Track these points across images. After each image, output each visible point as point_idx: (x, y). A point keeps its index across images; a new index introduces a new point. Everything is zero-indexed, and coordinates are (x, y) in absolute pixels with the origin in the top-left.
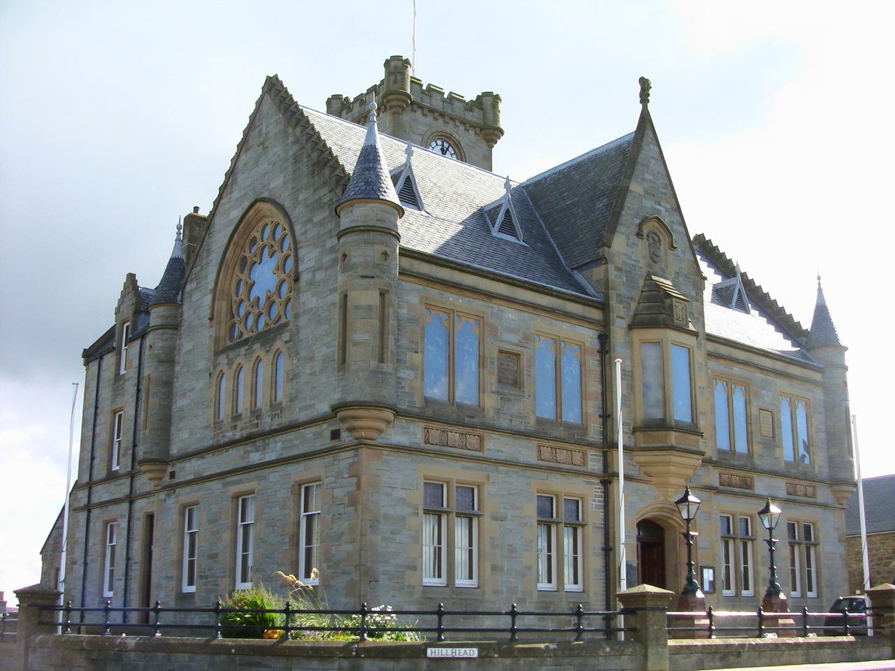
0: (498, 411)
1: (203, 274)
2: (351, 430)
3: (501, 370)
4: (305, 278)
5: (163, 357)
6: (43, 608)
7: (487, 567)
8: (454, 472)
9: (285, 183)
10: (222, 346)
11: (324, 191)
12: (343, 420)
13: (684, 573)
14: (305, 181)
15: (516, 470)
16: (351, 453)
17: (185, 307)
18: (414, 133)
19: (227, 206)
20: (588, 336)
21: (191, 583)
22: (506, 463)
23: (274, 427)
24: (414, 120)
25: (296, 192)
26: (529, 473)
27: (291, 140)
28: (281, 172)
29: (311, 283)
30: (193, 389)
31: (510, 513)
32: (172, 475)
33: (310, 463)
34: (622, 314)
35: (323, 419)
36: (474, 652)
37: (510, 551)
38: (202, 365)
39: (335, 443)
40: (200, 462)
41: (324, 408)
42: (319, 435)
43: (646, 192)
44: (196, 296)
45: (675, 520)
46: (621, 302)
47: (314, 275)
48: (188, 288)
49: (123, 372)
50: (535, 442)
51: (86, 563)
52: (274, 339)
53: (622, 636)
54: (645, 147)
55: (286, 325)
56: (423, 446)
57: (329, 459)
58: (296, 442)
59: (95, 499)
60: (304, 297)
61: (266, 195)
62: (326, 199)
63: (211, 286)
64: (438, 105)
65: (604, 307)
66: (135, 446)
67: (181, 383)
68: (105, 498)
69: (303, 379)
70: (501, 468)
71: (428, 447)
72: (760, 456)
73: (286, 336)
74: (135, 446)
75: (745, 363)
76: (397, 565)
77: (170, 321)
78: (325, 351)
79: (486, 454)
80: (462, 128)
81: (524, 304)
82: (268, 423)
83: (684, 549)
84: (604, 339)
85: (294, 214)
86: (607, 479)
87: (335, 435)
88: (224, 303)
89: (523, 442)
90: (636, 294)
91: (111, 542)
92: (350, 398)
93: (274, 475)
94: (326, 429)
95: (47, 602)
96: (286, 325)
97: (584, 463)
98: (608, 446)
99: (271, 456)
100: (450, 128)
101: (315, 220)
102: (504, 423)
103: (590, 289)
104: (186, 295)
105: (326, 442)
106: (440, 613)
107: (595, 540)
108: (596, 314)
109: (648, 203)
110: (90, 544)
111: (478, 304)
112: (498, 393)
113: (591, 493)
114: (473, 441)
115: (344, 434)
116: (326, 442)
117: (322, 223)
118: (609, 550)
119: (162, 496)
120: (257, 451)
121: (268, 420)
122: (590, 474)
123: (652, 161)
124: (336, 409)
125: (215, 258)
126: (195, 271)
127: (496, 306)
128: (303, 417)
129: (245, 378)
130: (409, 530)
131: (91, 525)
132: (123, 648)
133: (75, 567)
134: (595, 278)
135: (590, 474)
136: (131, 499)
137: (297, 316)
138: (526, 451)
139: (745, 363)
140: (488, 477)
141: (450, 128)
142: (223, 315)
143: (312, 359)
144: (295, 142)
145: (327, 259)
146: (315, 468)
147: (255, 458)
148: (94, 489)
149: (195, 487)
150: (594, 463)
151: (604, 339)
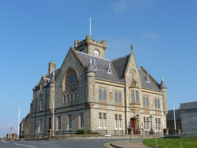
3: (110, 96)
7: (108, 125)
8: (103, 111)
13: (137, 126)
20: (123, 89)
26: (113, 111)
36: (110, 136)
45: (136, 111)
49: (42, 93)
51: (35, 127)
53: (128, 134)
54: (132, 57)
55: (77, 89)
56: (99, 108)
65: (125, 85)
66: (46, 106)
68: (39, 115)
72: (151, 107)
73: (77, 90)
74: (46, 106)
75: (148, 92)
79: (107, 109)
80: (92, 45)
82: (74, 104)
83: (137, 123)
84: (125, 90)
86: (126, 112)
90: (130, 82)
96: (77, 89)
97: (122, 110)
98: (126, 107)
99: (74, 109)
100: (97, 48)
102: (110, 104)
105: (84, 107)
106: (115, 131)
107: (124, 121)
108: (124, 86)
109: (132, 67)
110: (36, 123)
111: (106, 86)
113: (123, 114)
116: (84, 107)
118: (126, 123)
122: (123, 111)
127: (109, 86)
128: (80, 103)
129: (74, 99)
135: (123, 111)
136: (45, 115)
137: (79, 88)
138: (113, 108)
139: (148, 92)
143: (82, 95)
147: (71, 109)
150: (124, 109)
151: (125, 90)
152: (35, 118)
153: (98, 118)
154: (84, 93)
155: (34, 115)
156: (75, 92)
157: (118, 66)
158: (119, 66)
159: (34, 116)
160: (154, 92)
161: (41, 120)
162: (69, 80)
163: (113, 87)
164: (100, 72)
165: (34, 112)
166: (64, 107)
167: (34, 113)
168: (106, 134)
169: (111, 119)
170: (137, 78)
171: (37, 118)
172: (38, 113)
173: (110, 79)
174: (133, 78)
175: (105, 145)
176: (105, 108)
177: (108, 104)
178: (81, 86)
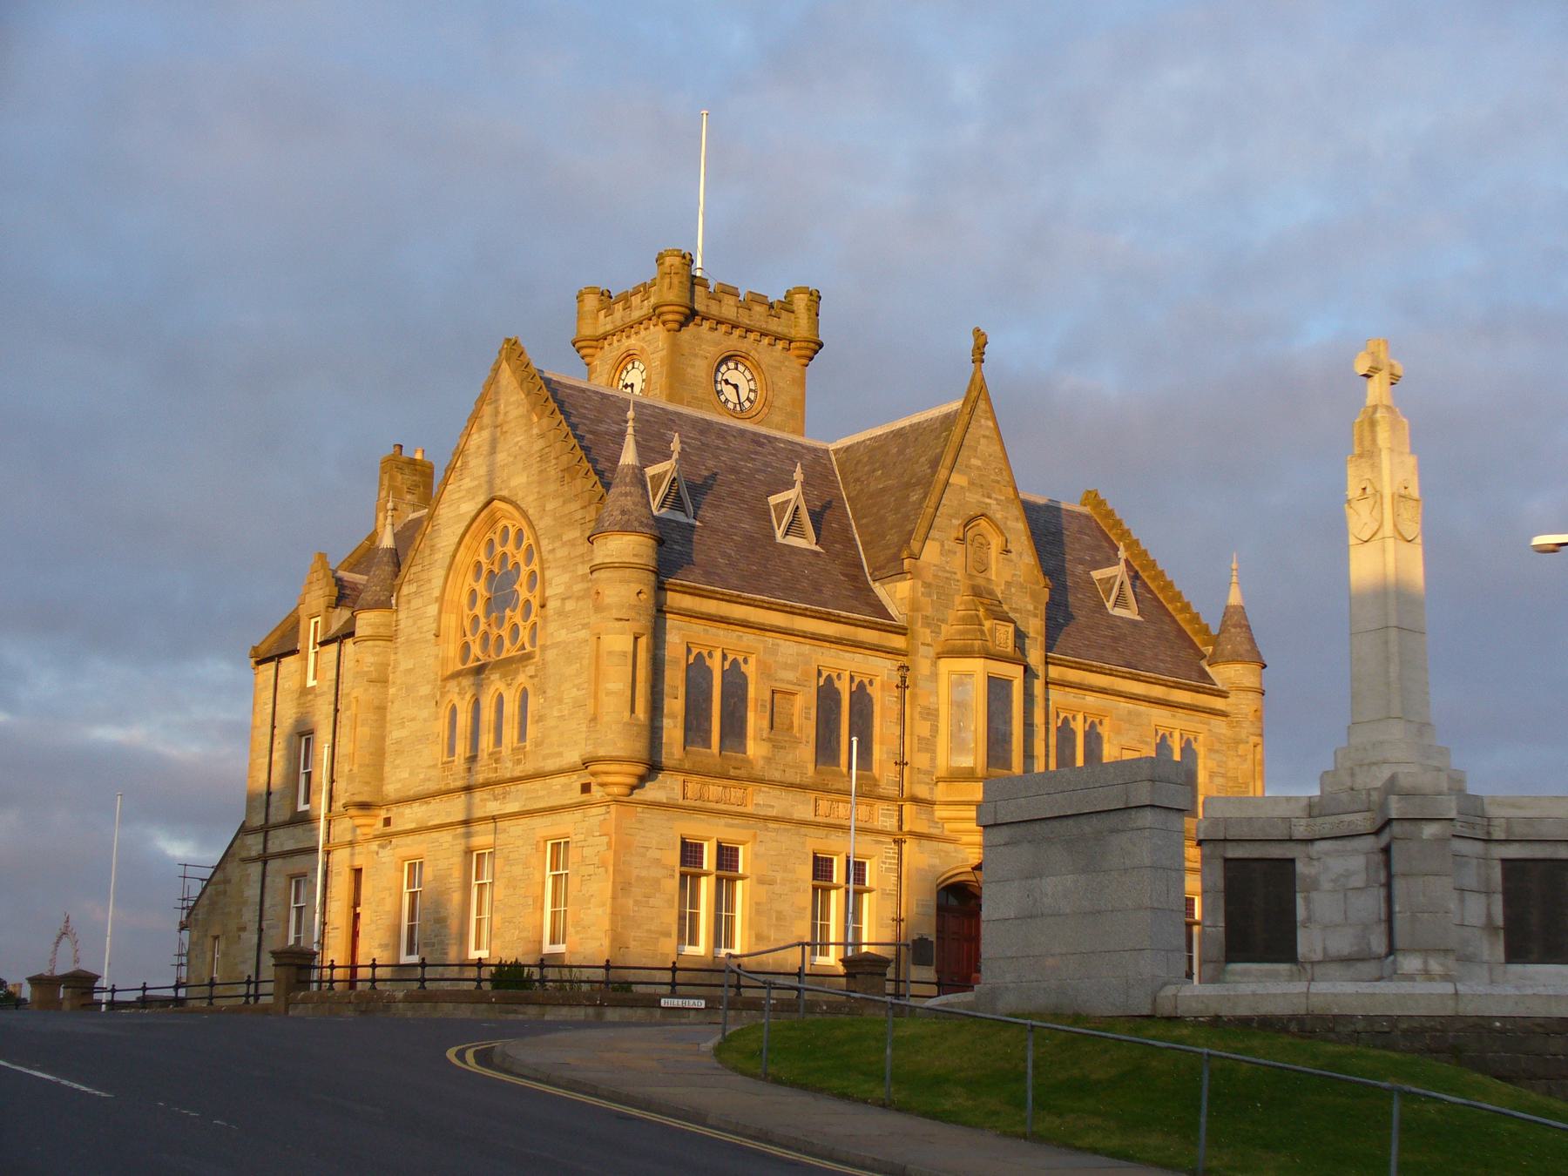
0: (768, 760)
1: (425, 576)
2: (602, 785)
4: (552, 605)
5: (374, 675)
6: (300, 967)
9: (528, 483)
10: (451, 669)
11: (574, 506)
12: (593, 774)
14: (552, 487)
15: (788, 826)
16: (603, 810)
17: (402, 615)
18: (696, 355)
19: (456, 496)
21: (410, 952)
22: (776, 819)
23: (517, 774)
24: (698, 338)
25: (542, 498)
26: (804, 830)
27: (535, 431)
28: (525, 469)
29: (561, 613)
30: (413, 719)
31: (779, 877)
32: (387, 822)
33: (556, 817)
34: (929, 640)
35: (573, 770)
36: (702, 1004)
37: (778, 919)
38: (425, 690)
39: (585, 797)
40: (424, 807)
41: (573, 757)
42: (567, 788)
43: (972, 483)
44: (416, 603)
46: (928, 625)
47: (563, 604)
48: (405, 590)
49: (311, 683)
50: (812, 795)
51: (261, 930)
52: (516, 672)
55: (529, 656)
56: (681, 801)
57: (578, 815)
58: (541, 793)
59: (274, 847)
60: (552, 627)
61: (505, 493)
62: (579, 515)
63: (437, 593)
64: (728, 309)
67: (395, 710)
68: (290, 845)
69: (551, 722)
70: (771, 825)
71: (686, 803)
73: (531, 670)
75: (1103, 691)
76: (649, 931)
77: (382, 631)
78: (574, 693)
79: (749, 809)
81: (805, 635)
85: (541, 525)
87: (586, 788)
88: (453, 617)
89: (799, 796)
91: (297, 901)
92: (601, 752)
93: (515, 829)
94: (576, 781)
95: (306, 962)
96: (529, 656)
100: (746, 345)
101: (565, 538)
102: (777, 775)
103: (892, 611)
104: (402, 600)
109: (973, 497)
110: (267, 905)
112: (769, 740)
114: (735, 794)
115: (594, 788)
116: (576, 796)
117: (572, 543)
119: (374, 846)
120: (496, 799)
121: (509, 764)
123: (983, 441)
124: (586, 764)
125: (442, 557)
126: (413, 570)
127: (770, 639)
128: (551, 765)
130: (1439, 769)
131: (268, 880)
132: (392, 999)
133: (244, 935)
134: (898, 596)
137: (544, 648)
138: (802, 808)
139: (1103, 691)
140: (755, 836)
141: (746, 345)
142: (452, 632)
143: (560, 701)
144: (542, 436)
145: (578, 587)
146: (565, 824)
148: (271, 833)
149: (417, 837)
152: (258, 867)
153: (672, 876)
154: (574, 693)
155: (254, 845)
156: (522, 678)
157: (873, 487)
158: (883, 490)
159: (254, 854)
160: (1157, 691)
161: (298, 883)
162: (489, 588)
163: (806, 648)
164: (715, 531)
165: (258, 820)
166: (443, 787)
167: (254, 831)
168: (673, 995)
169: (777, 888)
170: (1008, 584)
171: (273, 865)
172: (281, 832)
173: (789, 589)
174: (980, 581)
175: (451, 1054)
176: (721, 807)
177: (757, 772)
178: (562, 635)
